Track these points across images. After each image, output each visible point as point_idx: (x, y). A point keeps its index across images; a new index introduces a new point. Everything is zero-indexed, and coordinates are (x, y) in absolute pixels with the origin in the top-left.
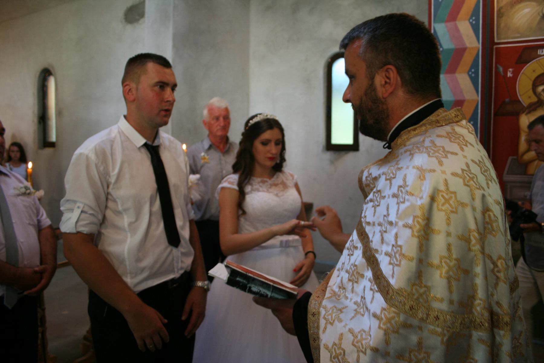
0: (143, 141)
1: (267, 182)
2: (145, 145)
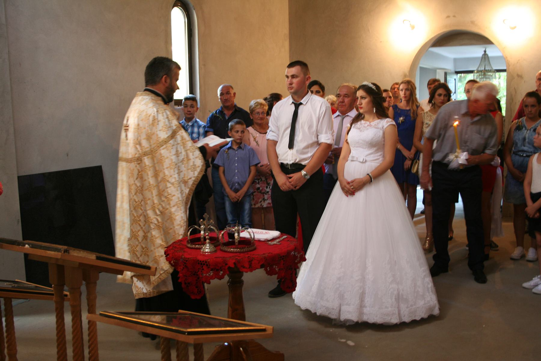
1: (367, 123)
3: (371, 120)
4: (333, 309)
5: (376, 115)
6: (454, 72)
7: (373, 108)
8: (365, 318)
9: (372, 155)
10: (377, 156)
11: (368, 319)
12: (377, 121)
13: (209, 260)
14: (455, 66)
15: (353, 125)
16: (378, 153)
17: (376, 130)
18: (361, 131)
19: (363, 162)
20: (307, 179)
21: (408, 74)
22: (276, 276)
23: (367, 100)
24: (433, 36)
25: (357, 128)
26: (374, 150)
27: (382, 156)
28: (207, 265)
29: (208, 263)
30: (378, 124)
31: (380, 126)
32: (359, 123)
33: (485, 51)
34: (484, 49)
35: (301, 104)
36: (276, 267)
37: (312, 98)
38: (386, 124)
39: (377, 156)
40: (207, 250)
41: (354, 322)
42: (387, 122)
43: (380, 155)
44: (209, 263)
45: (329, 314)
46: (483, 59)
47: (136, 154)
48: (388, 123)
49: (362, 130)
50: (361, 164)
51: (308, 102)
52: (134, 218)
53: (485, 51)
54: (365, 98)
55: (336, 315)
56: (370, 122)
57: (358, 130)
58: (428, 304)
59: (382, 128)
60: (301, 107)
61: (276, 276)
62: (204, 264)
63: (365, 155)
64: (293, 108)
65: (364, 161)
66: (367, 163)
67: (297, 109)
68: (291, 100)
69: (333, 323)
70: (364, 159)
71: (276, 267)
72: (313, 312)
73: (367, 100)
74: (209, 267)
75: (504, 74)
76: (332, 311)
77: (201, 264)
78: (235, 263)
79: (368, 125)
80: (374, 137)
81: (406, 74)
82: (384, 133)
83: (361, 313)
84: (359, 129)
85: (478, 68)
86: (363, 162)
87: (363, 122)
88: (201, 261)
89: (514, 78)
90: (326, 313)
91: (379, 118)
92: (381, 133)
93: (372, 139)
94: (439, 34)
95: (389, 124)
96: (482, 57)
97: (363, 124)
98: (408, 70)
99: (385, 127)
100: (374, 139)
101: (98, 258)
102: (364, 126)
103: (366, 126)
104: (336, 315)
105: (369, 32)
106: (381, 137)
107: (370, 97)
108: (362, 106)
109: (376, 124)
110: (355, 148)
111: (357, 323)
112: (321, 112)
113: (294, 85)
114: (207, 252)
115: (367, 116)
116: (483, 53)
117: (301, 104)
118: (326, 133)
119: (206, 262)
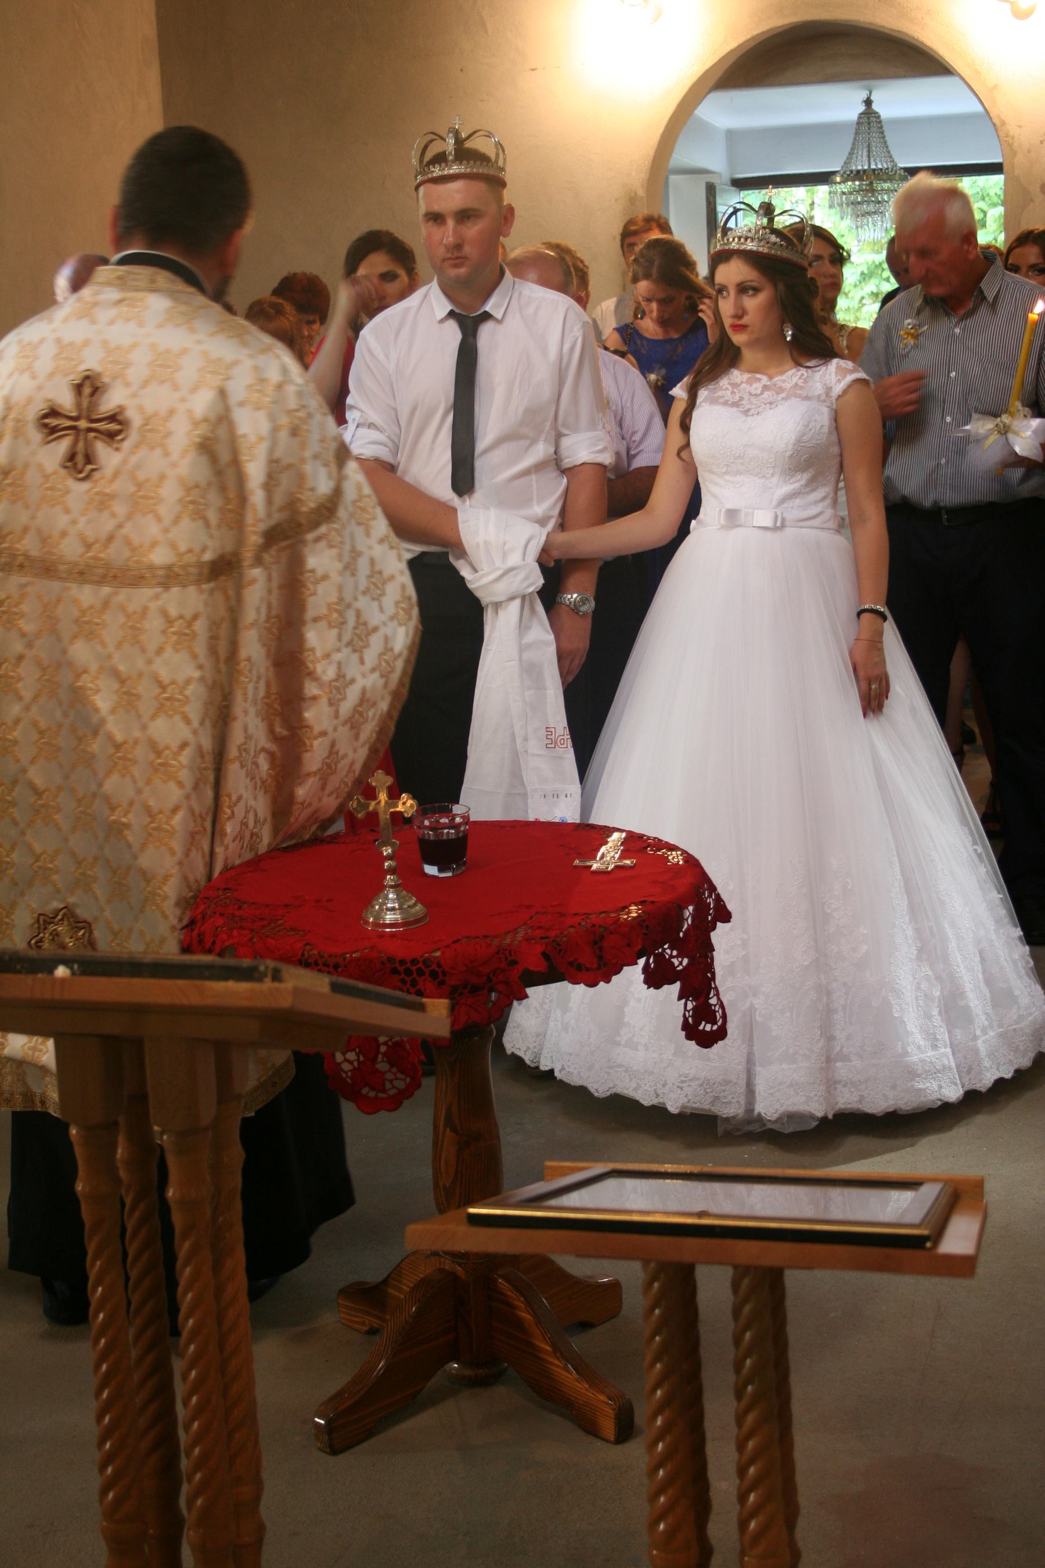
0: (448, 307)
1: (759, 380)
2: (452, 314)
3: (772, 371)
4: (727, 1082)
5: (791, 355)
6: (729, 182)
7: (783, 323)
8: (847, 1100)
9: (798, 501)
10: (816, 502)
11: (860, 1101)
12: (792, 376)
13: (438, 954)
14: (732, 160)
15: (703, 394)
16: (814, 490)
17: (806, 403)
18: (746, 413)
19: (775, 529)
20: (591, 614)
21: (641, 193)
22: (677, 986)
23: (762, 298)
24: (733, 44)
25: (725, 403)
26: (803, 482)
27: (828, 502)
28: (434, 975)
29: (434, 967)
30: (806, 381)
31: (818, 389)
32: (724, 382)
33: (868, 102)
34: (864, 95)
35: (487, 316)
36: (675, 953)
37: (520, 294)
38: (839, 381)
39: (816, 502)
40: (389, 917)
41: (812, 1117)
42: (845, 372)
43: (824, 498)
44: (439, 966)
45: (712, 1103)
46: (864, 128)
47: (204, 550)
48: (845, 377)
49: (749, 410)
50: (769, 535)
51: (510, 306)
52: (148, 820)
53: (868, 102)
54: (756, 290)
55: (738, 1102)
56: (771, 378)
57: (735, 409)
58: (1030, 1018)
59: (823, 397)
60: (486, 331)
61: (677, 986)
62: (420, 972)
63: (774, 503)
64: (453, 333)
65: (779, 524)
66: (789, 531)
67: (471, 339)
68: (441, 306)
69: (720, 1130)
70: (776, 517)
71: (675, 953)
72: (647, 1101)
73: (762, 298)
74: (442, 983)
75: (995, 183)
76: (724, 1091)
77: (408, 972)
78: (545, 955)
79: (765, 388)
80: (803, 435)
81: (636, 193)
82: (836, 418)
83: (831, 1084)
84: (735, 404)
85: (846, 163)
86: (775, 529)
87: (736, 375)
88: (402, 962)
89: (1032, 200)
90: (703, 1103)
91: (798, 364)
92: (824, 418)
93: (798, 441)
94: (747, 41)
95: (850, 378)
96: (859, 123)
97: (744, 385)
98: (644, 175)
99: (838, 389)
100: (806, 438)
101: (335, 988)
102: (750, 394)
103: (759, 392)
104: (738, 1102)
105: (486, 32)
106: (826, 430)
107: (775, 285)
108: (745, 320)
109: (800, 382)
110: (728, 477)
111: (824, 1120)
112: (567, 346)
113: (467, 250)
114: (391, 926)
115: (748, 355)
116: (862, 108)
117: (487, 316)
118: (592, 426)
119: (425, 962)
